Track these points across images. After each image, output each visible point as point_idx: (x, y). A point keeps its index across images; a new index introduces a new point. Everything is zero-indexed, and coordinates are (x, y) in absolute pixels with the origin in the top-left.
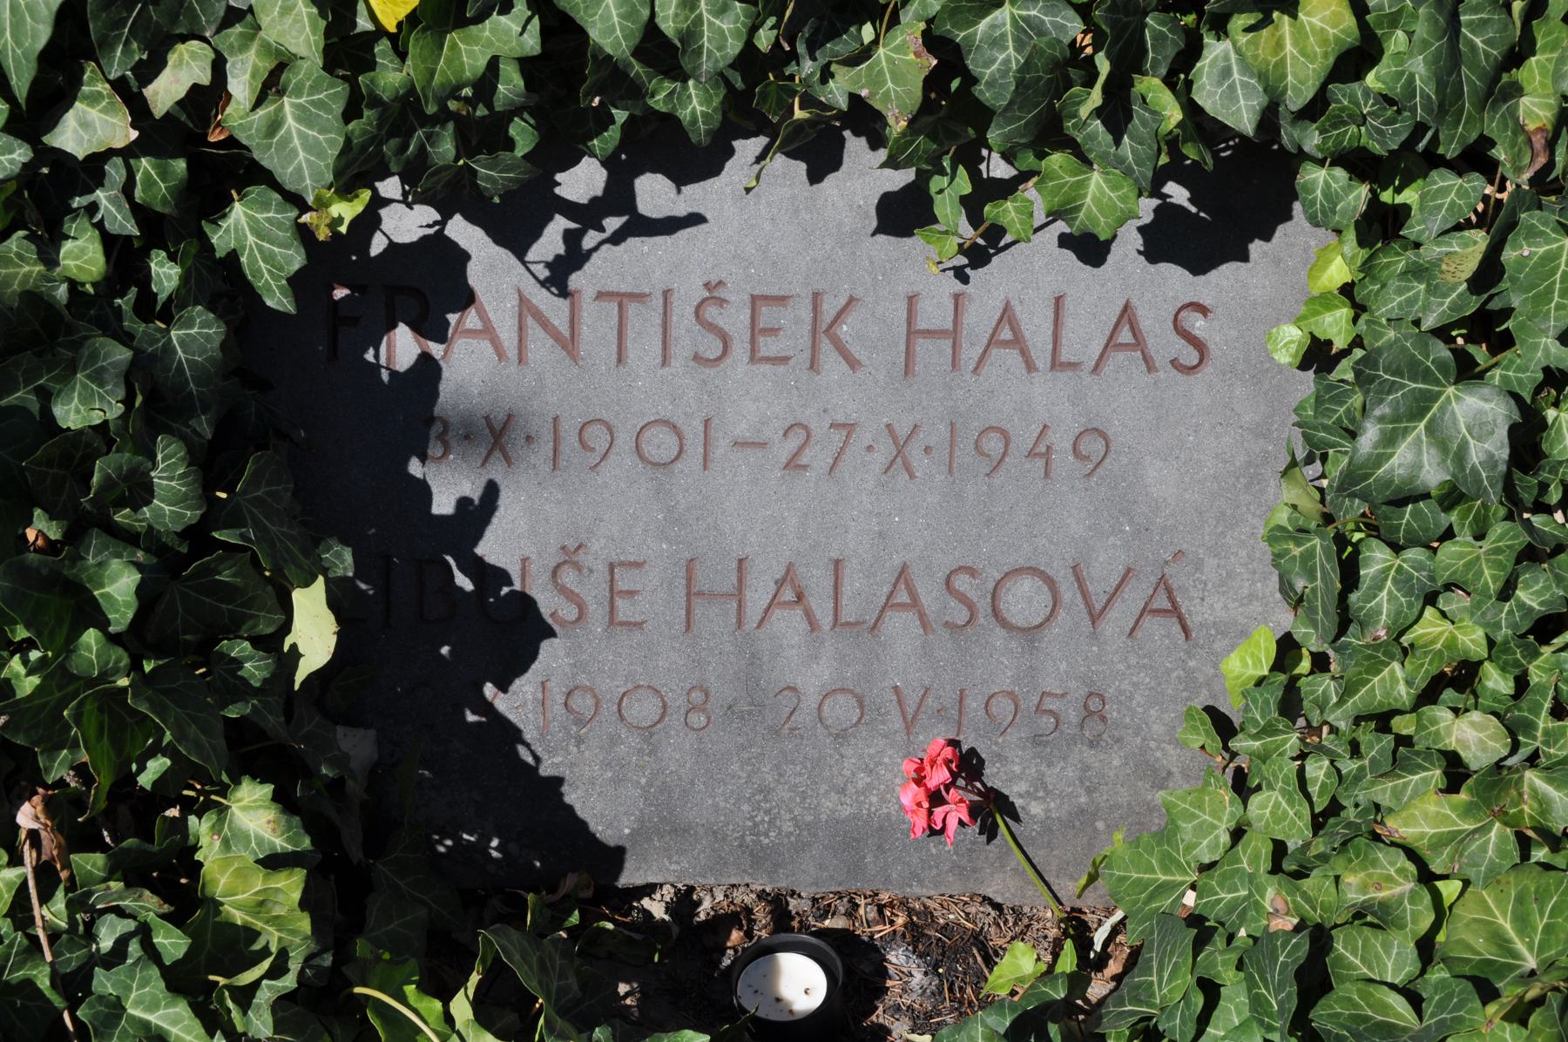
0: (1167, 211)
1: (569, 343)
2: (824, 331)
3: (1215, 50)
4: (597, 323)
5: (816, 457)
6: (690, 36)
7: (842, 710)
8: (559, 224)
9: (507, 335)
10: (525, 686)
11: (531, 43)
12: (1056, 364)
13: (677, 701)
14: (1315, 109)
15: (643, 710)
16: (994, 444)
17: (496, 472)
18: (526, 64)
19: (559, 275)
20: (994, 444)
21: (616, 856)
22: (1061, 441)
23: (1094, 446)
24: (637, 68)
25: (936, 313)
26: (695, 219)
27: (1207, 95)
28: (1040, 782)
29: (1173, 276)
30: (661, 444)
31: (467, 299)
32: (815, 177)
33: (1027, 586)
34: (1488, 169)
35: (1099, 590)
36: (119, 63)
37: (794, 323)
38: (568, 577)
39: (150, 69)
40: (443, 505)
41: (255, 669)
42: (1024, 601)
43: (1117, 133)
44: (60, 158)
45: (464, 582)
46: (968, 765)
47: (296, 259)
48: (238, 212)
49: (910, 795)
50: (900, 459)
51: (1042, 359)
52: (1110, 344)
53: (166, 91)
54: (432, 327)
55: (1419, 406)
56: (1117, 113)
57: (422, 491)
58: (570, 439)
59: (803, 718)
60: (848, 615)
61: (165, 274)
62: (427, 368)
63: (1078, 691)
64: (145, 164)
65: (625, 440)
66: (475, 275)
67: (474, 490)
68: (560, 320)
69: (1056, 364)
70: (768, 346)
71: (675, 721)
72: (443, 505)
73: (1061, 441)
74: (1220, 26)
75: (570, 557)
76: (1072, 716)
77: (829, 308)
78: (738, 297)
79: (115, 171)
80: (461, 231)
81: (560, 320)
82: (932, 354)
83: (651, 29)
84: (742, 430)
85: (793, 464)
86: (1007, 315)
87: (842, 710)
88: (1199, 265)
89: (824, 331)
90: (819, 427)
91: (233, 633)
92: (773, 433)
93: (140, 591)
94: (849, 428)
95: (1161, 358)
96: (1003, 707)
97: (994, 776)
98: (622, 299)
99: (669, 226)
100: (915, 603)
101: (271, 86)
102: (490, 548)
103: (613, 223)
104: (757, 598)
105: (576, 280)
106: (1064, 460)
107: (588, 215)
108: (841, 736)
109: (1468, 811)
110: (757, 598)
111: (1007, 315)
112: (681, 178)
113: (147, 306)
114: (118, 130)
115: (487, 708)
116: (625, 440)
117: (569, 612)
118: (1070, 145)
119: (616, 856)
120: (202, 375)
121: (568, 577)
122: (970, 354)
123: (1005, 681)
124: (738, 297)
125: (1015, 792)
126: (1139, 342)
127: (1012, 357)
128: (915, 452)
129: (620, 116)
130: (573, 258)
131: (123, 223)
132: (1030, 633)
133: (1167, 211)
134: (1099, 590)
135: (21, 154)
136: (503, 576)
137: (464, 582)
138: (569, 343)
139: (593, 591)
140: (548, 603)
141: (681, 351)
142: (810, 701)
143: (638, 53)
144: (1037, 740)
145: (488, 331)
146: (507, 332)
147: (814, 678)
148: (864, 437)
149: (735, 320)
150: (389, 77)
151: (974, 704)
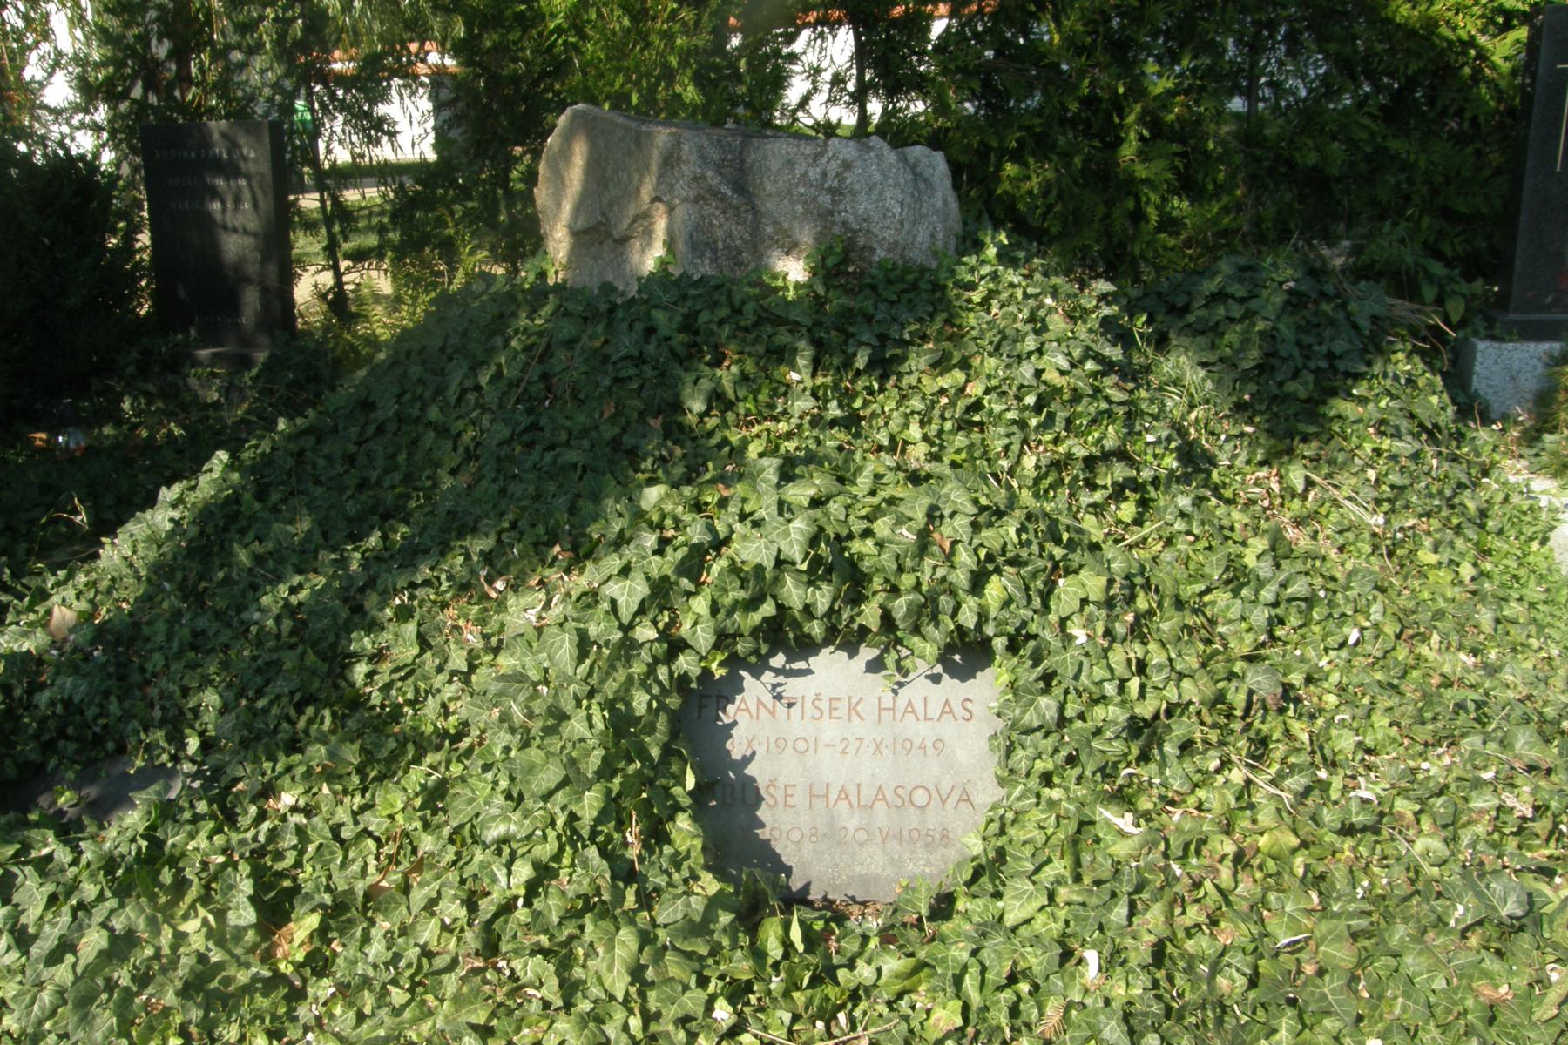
2: (852, 708)
5: (851, 749)
7: (862, 835)
12: (926, 719)
13: (807, 832)
16: (908, 745)
20: (908, 745)
22: (929, 744)
23: (939, 745)
30: (801, 745)
32: (851, 657)
33: (920, 792)
35: (944, 793)
36: (651, 614)
37: (843, 707)
38: (772, 790)
42: (920, 797)
48: (682, 658)
51: (922, 717)
52: (943, 712)
65: (790, 744)
69: (926, 719)
70: (835, 714)
71: (806, 840)
73: (929, 744)
76: (938, 836)
78: (825, 698)
82: (886, 715)
84: (827, 741)
86: (910, 703)
89: (852, 708)
90: (852, 739)
94: (861, 740)
100: (884, 799)
104: (833, 797)
106: (930, 750)
108: (862, 844)
111: (910, 703)
116: (790, 744)
122: (899, 715)
123: (915, 825)
124: (825, 698)
126: (951, 712)
132: (923, 808)
134: (944, 793)
139: (779, 795)
141: (808, 715)
142: (851, 832)
144: (927, 845)
147: (852, 824)
148: (866, 743)
149: (825, 705)
151: (905, 833)
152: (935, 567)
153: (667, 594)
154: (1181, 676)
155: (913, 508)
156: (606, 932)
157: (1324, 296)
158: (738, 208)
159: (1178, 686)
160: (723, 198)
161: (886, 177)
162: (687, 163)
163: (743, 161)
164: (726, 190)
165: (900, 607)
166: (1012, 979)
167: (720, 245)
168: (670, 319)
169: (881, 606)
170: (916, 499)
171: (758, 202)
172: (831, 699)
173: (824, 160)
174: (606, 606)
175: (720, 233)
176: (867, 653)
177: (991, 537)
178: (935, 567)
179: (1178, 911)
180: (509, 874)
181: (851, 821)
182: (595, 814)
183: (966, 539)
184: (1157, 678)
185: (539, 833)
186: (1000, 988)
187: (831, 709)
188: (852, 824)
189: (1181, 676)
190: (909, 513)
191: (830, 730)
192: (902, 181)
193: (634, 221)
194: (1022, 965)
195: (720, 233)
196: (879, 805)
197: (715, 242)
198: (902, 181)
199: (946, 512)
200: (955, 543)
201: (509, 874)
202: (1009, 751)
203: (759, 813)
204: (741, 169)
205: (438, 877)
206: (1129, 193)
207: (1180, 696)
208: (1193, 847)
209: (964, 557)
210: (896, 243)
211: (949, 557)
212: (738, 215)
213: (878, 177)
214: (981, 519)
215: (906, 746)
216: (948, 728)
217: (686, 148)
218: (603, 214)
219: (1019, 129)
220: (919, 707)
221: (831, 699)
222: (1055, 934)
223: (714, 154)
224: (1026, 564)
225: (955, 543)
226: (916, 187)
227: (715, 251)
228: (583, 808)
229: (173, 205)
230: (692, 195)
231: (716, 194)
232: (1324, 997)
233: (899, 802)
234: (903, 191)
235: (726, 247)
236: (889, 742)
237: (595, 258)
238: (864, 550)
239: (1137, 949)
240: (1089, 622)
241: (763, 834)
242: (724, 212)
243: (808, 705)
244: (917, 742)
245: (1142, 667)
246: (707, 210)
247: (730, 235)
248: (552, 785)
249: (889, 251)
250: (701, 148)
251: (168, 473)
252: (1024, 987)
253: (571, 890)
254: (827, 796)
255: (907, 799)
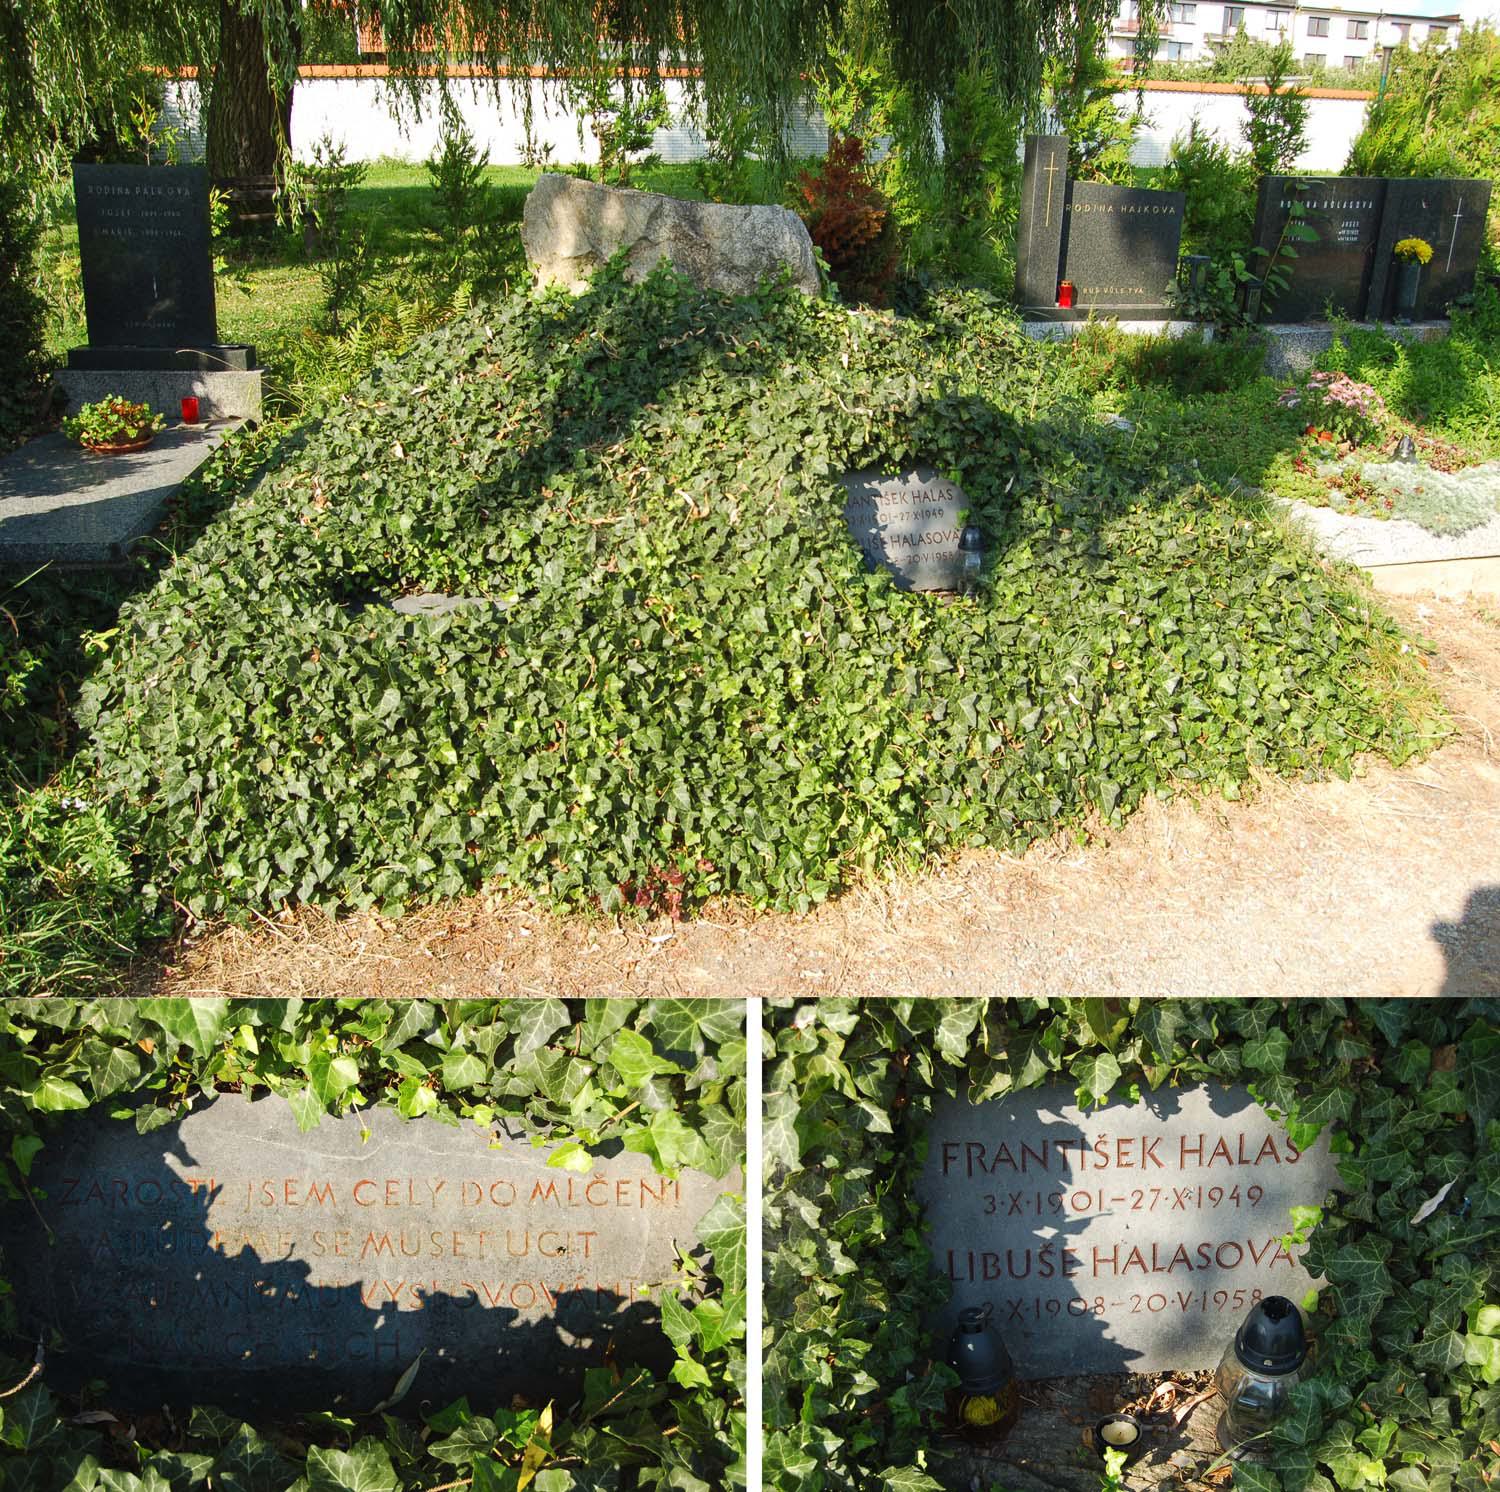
5: (1146, 1203)
16: (1216, 1195)
52: (1263, 1153)
69: (1241, 1161)
70: (1125, 1160)
73: (1243, 1192)
106: (1244, 1199)
157: (929, 610)
172: (1120, 1141)
187: (1120, 1154)
203: (265, 1260)
221: (1120, 1141)
229: (219, 264)
233: (1204, 1262)
241: (1107, 1334)
251: (1385, 1009)
255: (1213, 1257)
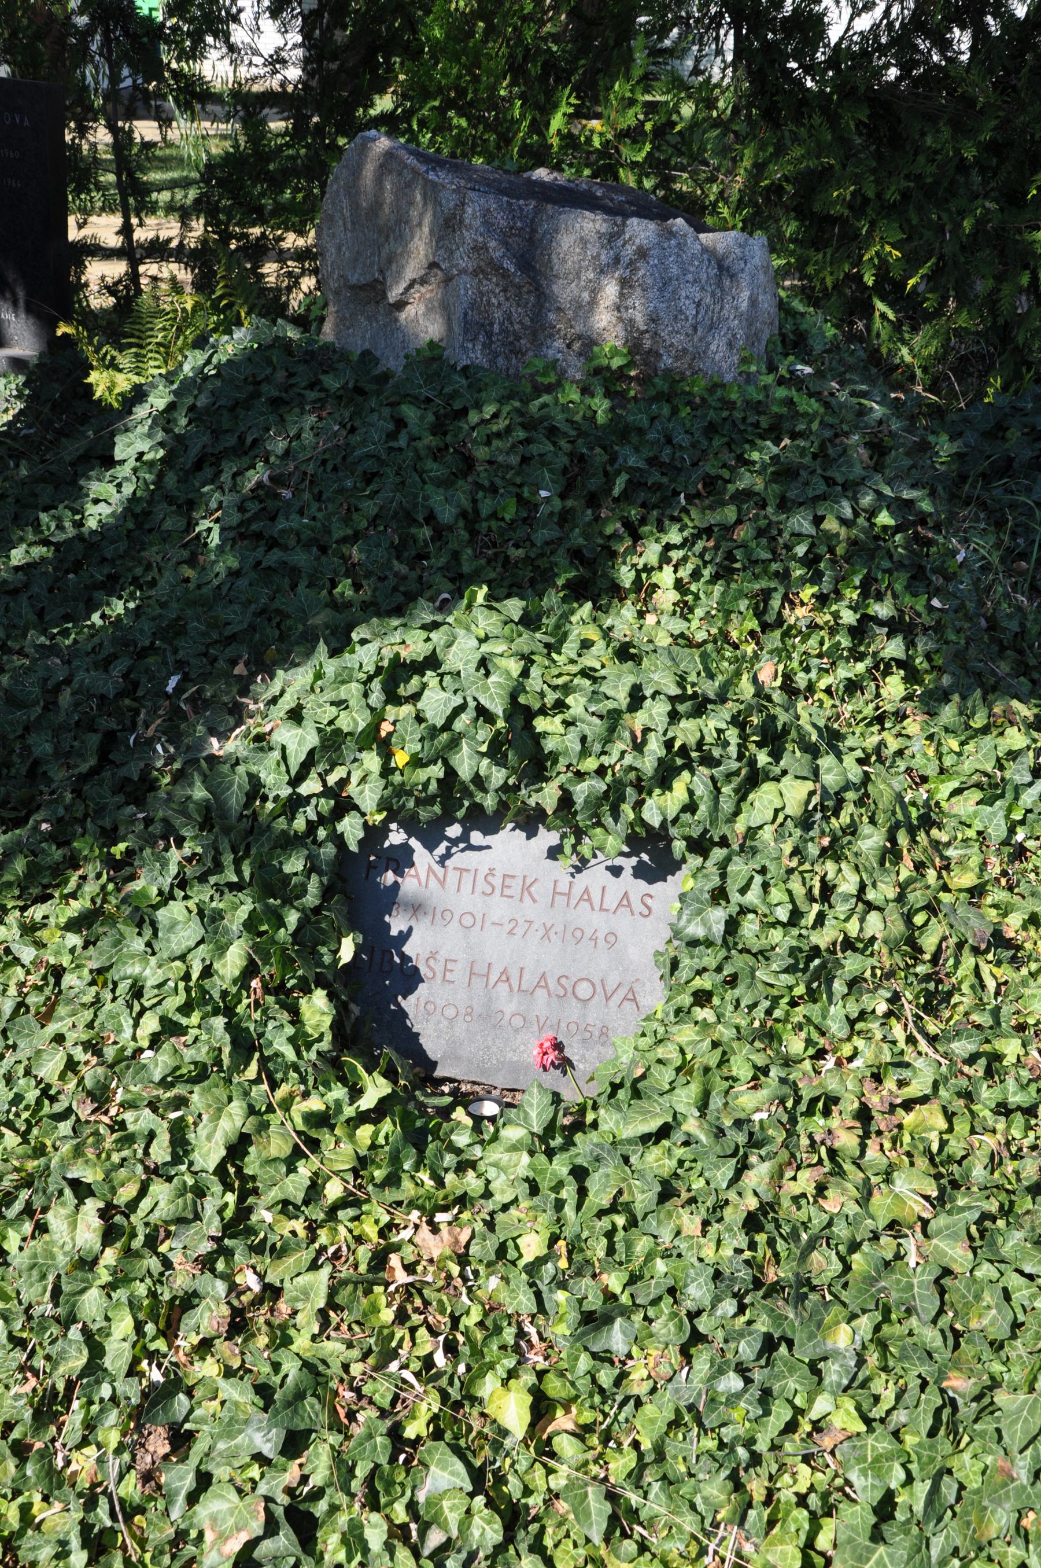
0: (641, 862)
1: (442, 883)
2: (526, 889)
3: (649, 802)
4: (452, 877)
5: (519, 931)
6: (488, 777)
7: (518, 1021)
8: (445, 844)
9: (423, 878)
10: (412, 998)
11: (441, 775)
12: (601, 909)
13: (462, 1011)
14: (675, 821)
15: (450, 1012)
16: (578, 934)
17: (413, 923)
18: (438, 780)
19: (443, 860)
20: (578, 934)
21: (434, 1065)
22: (601, 936)
23: (612, 939)
24: (472, 787)
25: (563, 887)
26: (488, 847)
27: (646, 815)
28: (583, 1056)
29: (642, 883)
30: (468, 921)
31: (412, 865)
32: (528, 838)
33: (585, 985)
34: (728, 846)
35: (610, 989)
36: (321, 768)
37: (516, 885)
38: (431, 962)
39: (327, 772)
40: (394, 932)
41: (327, 959)
42: (584, 990)
43: (616, 820)
44: (299, 795)
45: (397, 960)
46: (558, 1046)
47: (361, 834)
48: (346, 820)
49: (536, 1051)
50: (546, 935)
51: (597, 907)
52: (620, 905)
53: (332, 779)
54: (399, 872)
55: (699, 912)
56: (616, 814)
57: (388, 927)
58: (439, 915)
59: (504, 1022)
60: (524, 987)
61: (322, 833)
62: (396, 886)
63: (599, 1025)
64: (322, 800)
65: (456, 918)
66: (416, 858)
67: (405, 929)
68: (441, 875)
69: (601, 909)
70: (507, 892)
71: (460, 1018)
72: (394, 932)
73: (601, 936)
74: (650, 794)
75: (433, 955)
76: (597, 1033)
77: (528, 882)
78: (499, 874)
79: (314, 801)
80: (414, 843)
81: (441, 875)
82: (561, 900)
83: (477, 774)
84: (495, 919)
85: (511, 933)
86: (586, 891)
87: (518, 1021)
88: (651, 882)
89: (526, 889)
90: (521, 921)
91: (323, 944)
92: (505, 921)
93: (299, 920)
94: (531, 922)
95: (636, 911)
96: (573, 1027)
97: (567, 1053)
98: (462, 870)
99: (480, 848)
100: (546, 986)
101: (363, 780)
102: (407, 949)
103: (462, 845)
104: (493, 978)
105: (448, 863)
106: (601, 942)
107: (454, 842)
108: (517, 1031)
109: (698, 1033)
110: (493, 978)
111: (586, 891)
112: (486, 832)
113: (315, 841)
114: (318, 788)
115: (398, 1005)
116: (456, 918)
117: (430, 975)
118: (603, 826)
119: (434, 1065)
120: (327, 864)
121: (431, 962)
122: (573, 902)
123: (574, 1018)
124: (499, 874)
125: (574, 1059)
126: (629, 905)
127: (587, 905)
128: (552, 934)
129: (466, 803)
130: (448, 855)
131: (313, 817)
132: (585, 1001)
133: (641, 862)
134: (610, 989)
135: (290, 790)
136: (410, 959)
137: (397, 960)
138: (442, 883)
139: (439, 968)
140: (423, 971)
141: (478, 889)
142: (507, 1017)
143: (473, 781)
144: (584, 1040)
145: (417, 876)
146: (423, 877)
147: (509, 1008)
148: (535, 926)
149: (497, 881)
150: (397, 778)
151: (563, 1025)
152: (623, 753)
153: (339, 747)
154: (870, 906)
155: (616, 687)
156: (218, 1100)
158: (520, 287)
159: (862, 920)
160: (505, 275)
161: (685, 272)
162: (469, 228)
163: (534, 231)
164: (509, 265)
165: (581, 791)
166: (613, 1208)
167: (496, 328)
168: (422, 418)
169: (561, 787)
170: (619, 677)
171: (544, 283)
173: (620, 242)
174: (276, 754)
175: (498, 315)
176: (548, 838)
177: (687, 731)
178: (623, 753)
179: (789, 1174)
180: (136, 1025)
181: (508, 1004)
182: (237, 973)
183: (661, 730)
184: (841, 909)
185: (171, 984)
186: (601, 1213)
188: (509, 1008)
189: (870, 906)
190: (610, 693)
191: (499, 908)
192: (704, 277)
193: (411, 286)
194: (625, 1198)
195: (498, 315)
196: (541, 993)
197: (492, 324)
198: (704, 277)
199: (648, 692)
200: (646, 730)
201: (136, 1025)
202: (675, 965)
204: (531, 240)
205: (73, 1014)
206: (1026, 267)
207: (861, 930)
208: (820, 1105)
209: (655, 747)
210: (685, 351)
211: (639, 747)
212: (519, 295)
213: (675, 270)
214: (681, 708)
215: (577, 935)
216: (623, 923)
217: (469, 210)
218: (381, 272)
219: (907, 177)
220: (596, 896)
222: (666, 1173)
223: (501, 220)
224: (718, 763)
225: (646, 730)
226: (719, 285)
227: (489, 335)
228: (224, 966)
230: (471, 266)
231: (497, 268)
232: (910, 1286)
234: (703, 289)
235: (502, 331)
236: (560, 928)
237: (369, 318)
238: (550, 728)
239: (736, 1206)
240: (780, 835)
242: (505, 290)
243: (480, 878)
244: (588, 933)
245: (827, 890)
246: (487, 286)
247: (509, 318)
248: (192, 943)
249: (677, 358)
250: (486, 212)
252: (620, 1220)
253: (189, 1054)
254: (487, 976)
